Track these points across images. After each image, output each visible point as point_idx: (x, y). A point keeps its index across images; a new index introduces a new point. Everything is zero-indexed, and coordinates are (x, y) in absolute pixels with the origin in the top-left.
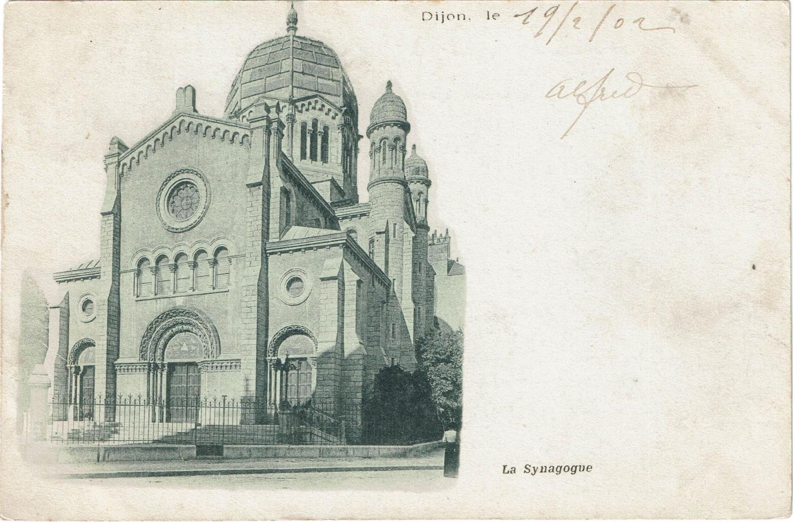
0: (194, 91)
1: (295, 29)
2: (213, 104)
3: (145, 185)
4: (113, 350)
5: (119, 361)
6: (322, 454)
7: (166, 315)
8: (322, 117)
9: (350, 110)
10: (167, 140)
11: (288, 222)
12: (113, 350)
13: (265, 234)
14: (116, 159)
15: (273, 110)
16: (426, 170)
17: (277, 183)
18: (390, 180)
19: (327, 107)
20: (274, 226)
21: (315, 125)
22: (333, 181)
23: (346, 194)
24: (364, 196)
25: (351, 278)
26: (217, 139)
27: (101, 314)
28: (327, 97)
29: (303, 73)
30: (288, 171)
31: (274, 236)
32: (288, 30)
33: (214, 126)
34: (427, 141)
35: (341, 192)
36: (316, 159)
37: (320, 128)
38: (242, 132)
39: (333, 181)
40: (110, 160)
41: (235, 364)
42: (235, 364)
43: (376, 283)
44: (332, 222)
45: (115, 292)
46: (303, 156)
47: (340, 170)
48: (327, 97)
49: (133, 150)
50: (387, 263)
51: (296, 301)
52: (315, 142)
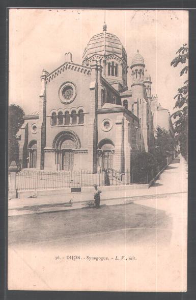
0: (71, 55)
1: (106, 30)
2: (78, 59)
3: (54, 89)
4: (43, 144)
5: (46, 148)
6: (117, 189)
7: (61, 133)
8: (115, 61)
9: (125, 58)
10: (56, 75)
11: (104, 101)
12: (43, 144)
13: (96, 106)
14: (44, 77)
15: (98, 62)
16: (150, 78)
17: (100, 88)
18: (139, 84)
19: (117, 58)
20: (99, 103)
21: (113, 64)
22: (119, 84)
23: (123, 88)
24: (129, 88)
25: (126, 122)
26: (76, 71)
27: (39, 130)
28: (117, 55)
29: (109, 46)
30: (104, 83)
31: (99, 107)
32: (104, 30)
33: (78, 67)
34: (149, 71)
35: (122, 87)
36: (134, 183)
37: (115, 65)
38: (88, 70)
39: (119, 84)
40: (42, 77)
41: (85, 152)
42: (85, 152)
43: (135, 121)
44: (119, 98)
45: (44, 123)
46: (109, 74)
47: (121, 79)
48: (117, 55)
49: (50, 74)
50: (138, 114)
51: (107, 130)
52: (113, 70)
